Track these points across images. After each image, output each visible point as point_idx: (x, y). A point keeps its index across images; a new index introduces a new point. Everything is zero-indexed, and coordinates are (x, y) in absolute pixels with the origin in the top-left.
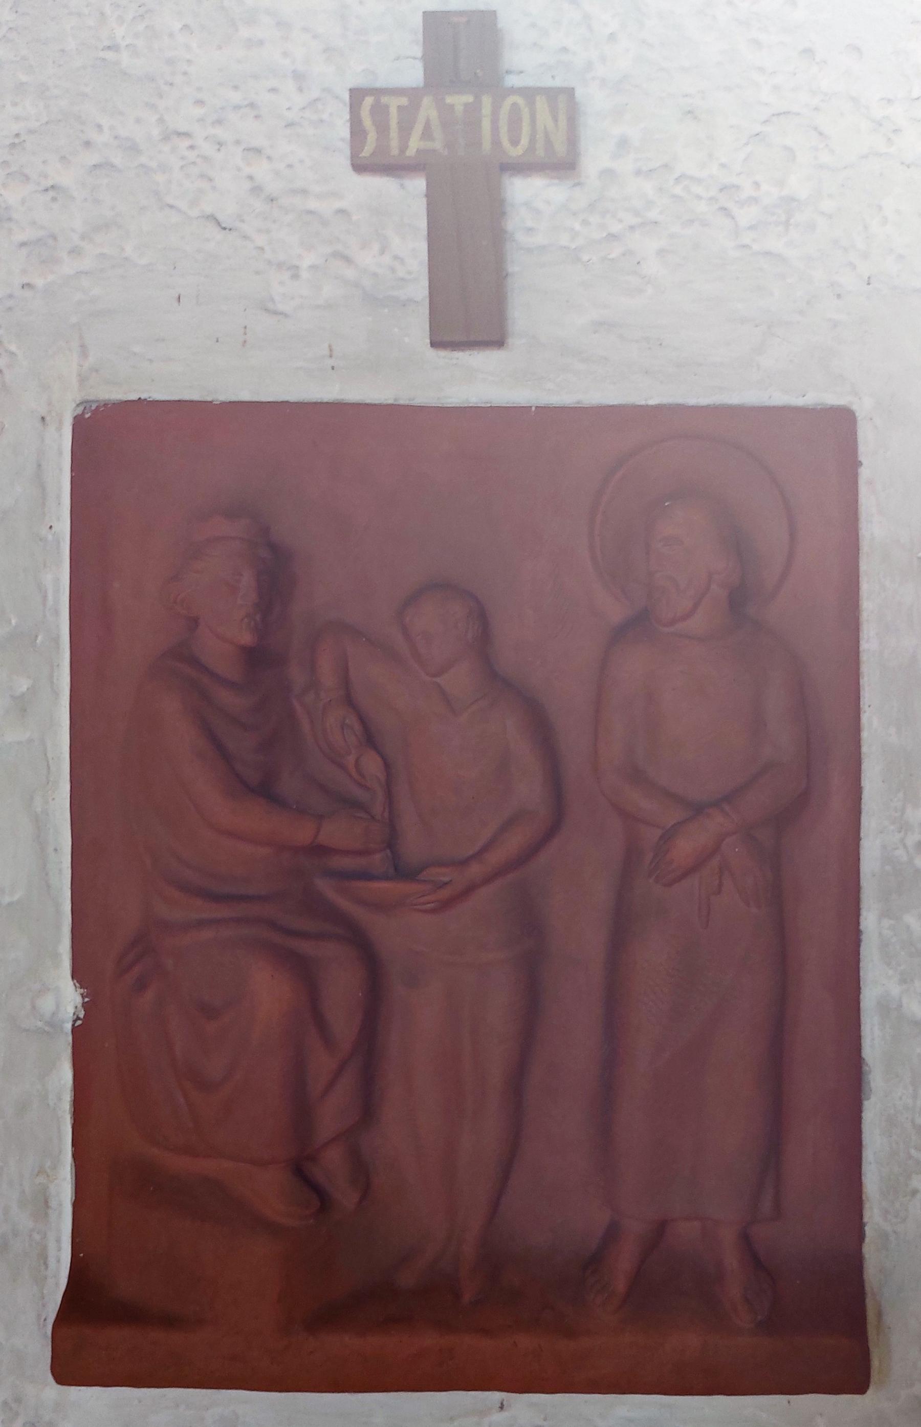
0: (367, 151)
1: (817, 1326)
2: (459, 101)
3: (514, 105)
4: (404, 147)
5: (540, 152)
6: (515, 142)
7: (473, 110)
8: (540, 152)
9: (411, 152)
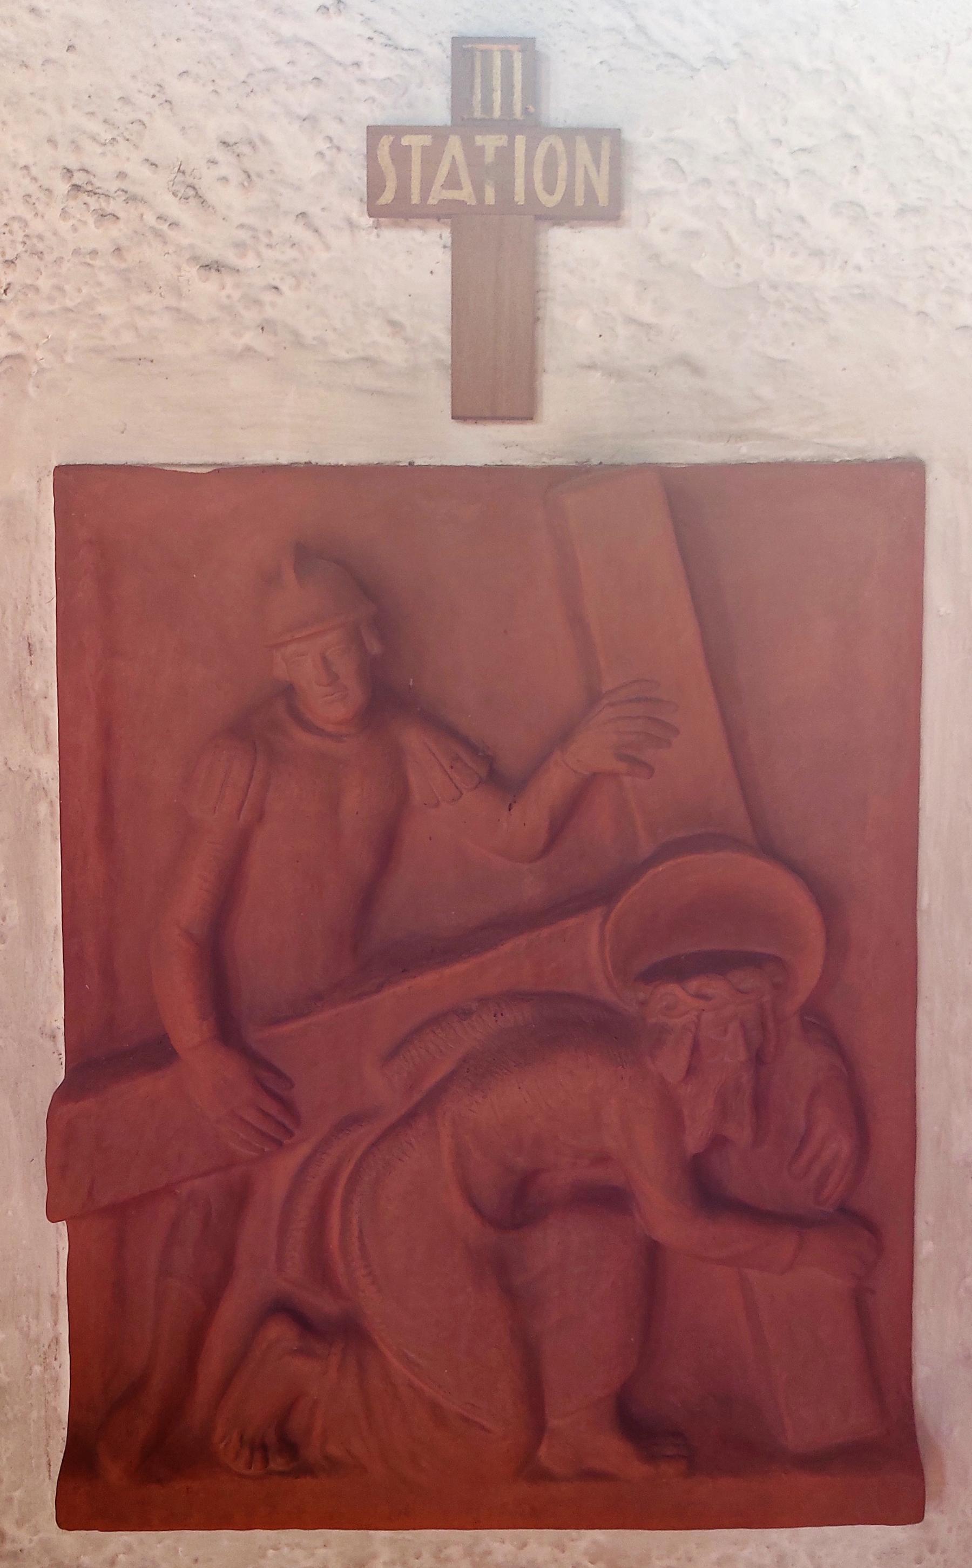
0: (387, 197)
1: (880, 1468)
2: (490, 143)
3: (551, 192)
4: (426, 191)
5: (580, 201)
6: (550, 191)
7: (505, 155)
8: (580, 201)
9: (432, 201)
